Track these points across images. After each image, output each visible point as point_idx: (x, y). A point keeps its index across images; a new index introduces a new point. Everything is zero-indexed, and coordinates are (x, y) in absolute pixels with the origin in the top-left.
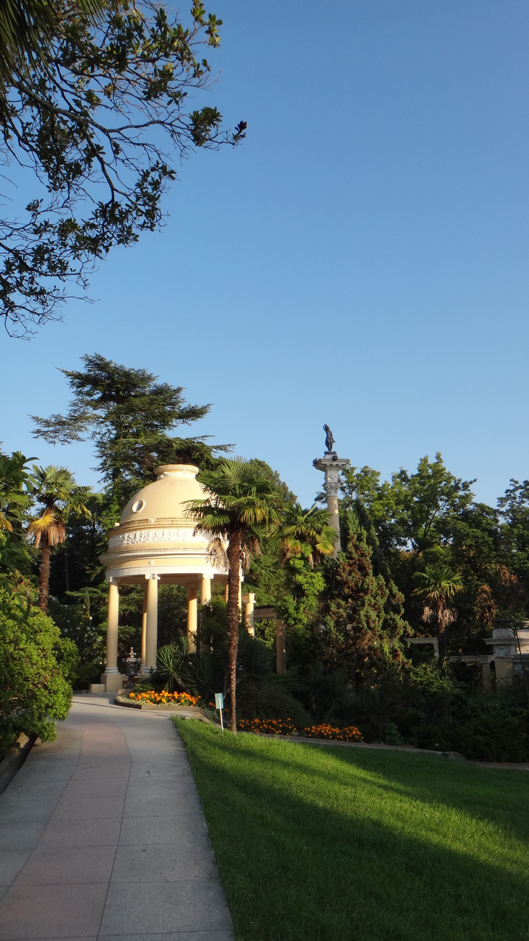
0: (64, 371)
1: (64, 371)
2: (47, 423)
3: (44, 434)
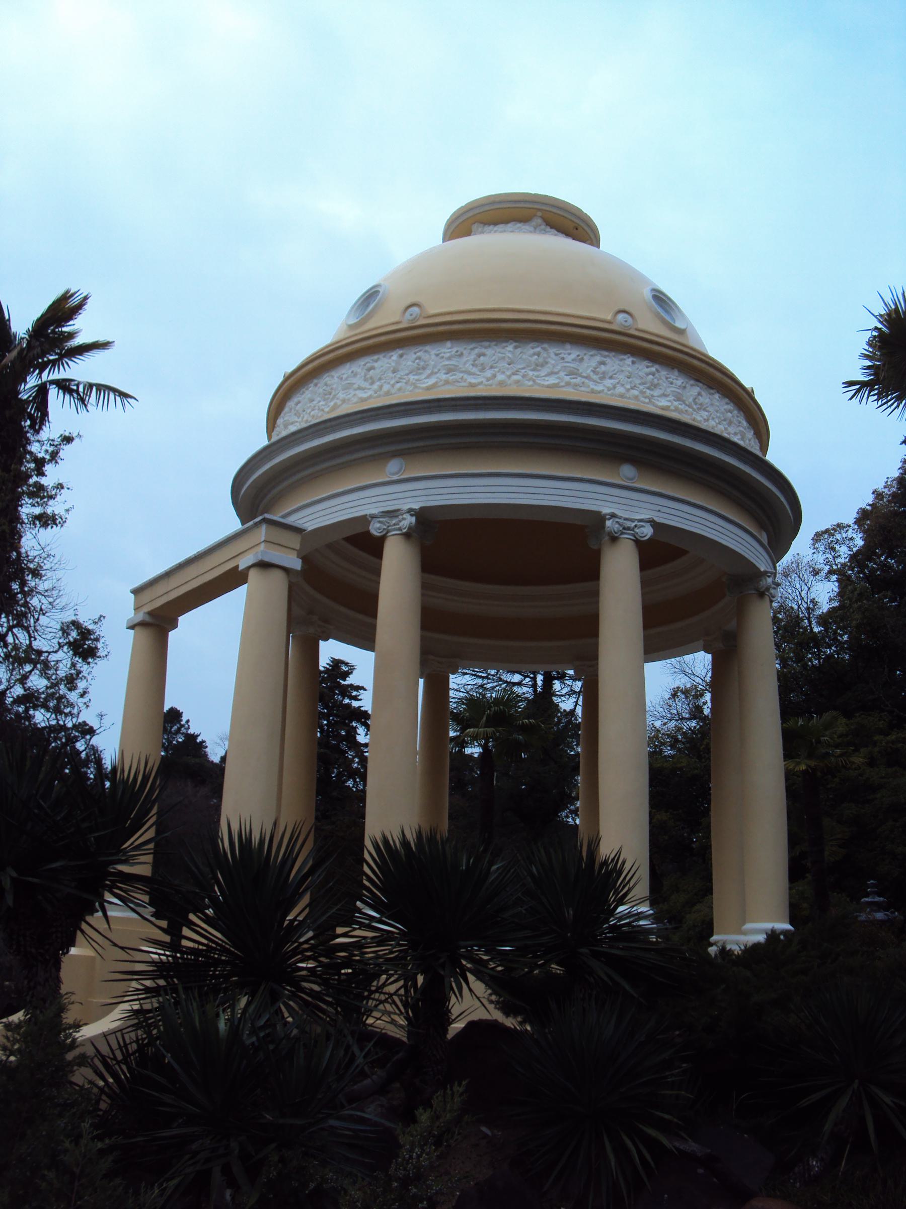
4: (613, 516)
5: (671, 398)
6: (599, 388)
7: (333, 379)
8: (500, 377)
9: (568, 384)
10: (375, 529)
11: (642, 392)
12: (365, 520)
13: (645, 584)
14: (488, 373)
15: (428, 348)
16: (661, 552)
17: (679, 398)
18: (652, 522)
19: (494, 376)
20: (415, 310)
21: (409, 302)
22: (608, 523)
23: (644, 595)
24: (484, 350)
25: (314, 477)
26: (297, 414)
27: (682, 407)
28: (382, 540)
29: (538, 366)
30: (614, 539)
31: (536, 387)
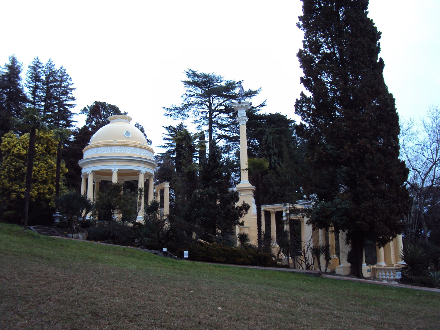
0: (183, 81)
1: (183, 81)
2: (171, 110)
3: (171, 115)
12: (111, 170)
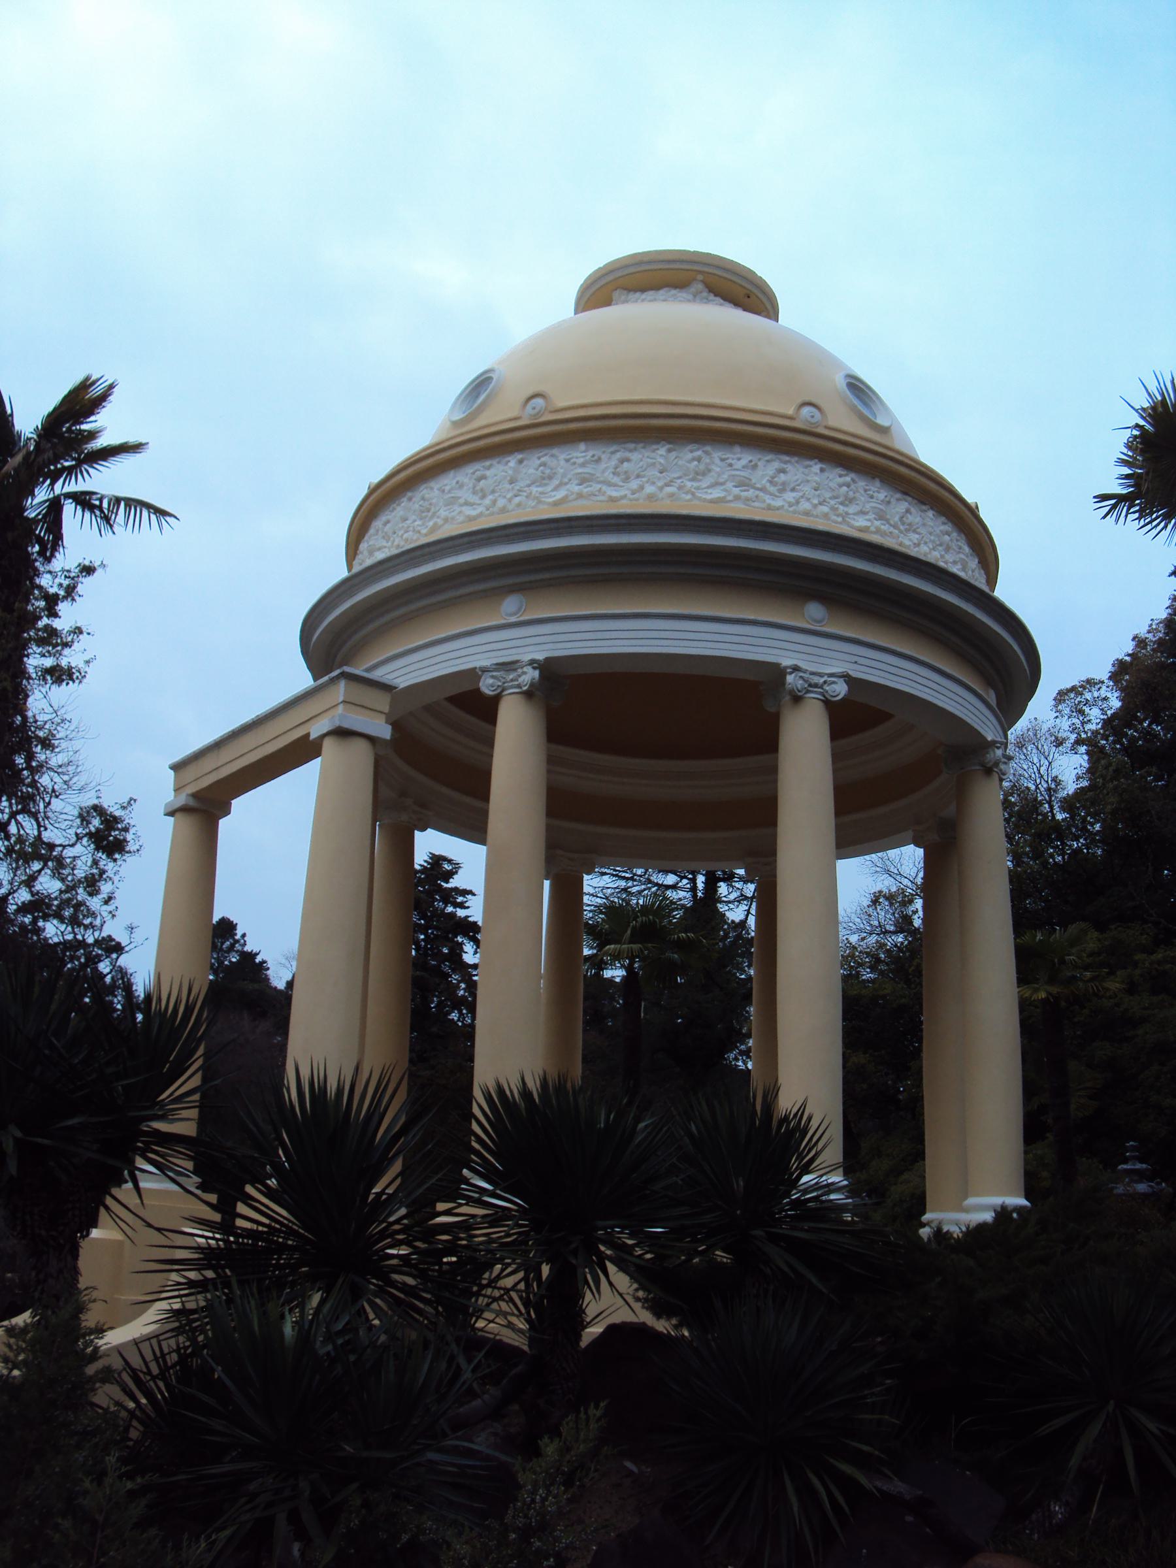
4: (796, 669)
5: (871, 516)
6: (778, 503)
7: (432, 492)
8: (649, 489)
9: (737, 498)
10: (487, 686)
11: (833, 509)
12: (473, 674)
13: (837, 757)
14: (634, 484)
15: (555, 451)
16: (858, 715)
17: (881, 516)
18: (847, 678)
19: (642, 488)
20: (539, 402)
21: (530, 392)
22: (790, 679)
23: (835, 771)
24: (628, 454)
25: (408, 619)
26: (386, 537)
27: (885, 528)
28: (495, 700)
29: (698, 475)
30: (797, 699)
31: (696, 502)
